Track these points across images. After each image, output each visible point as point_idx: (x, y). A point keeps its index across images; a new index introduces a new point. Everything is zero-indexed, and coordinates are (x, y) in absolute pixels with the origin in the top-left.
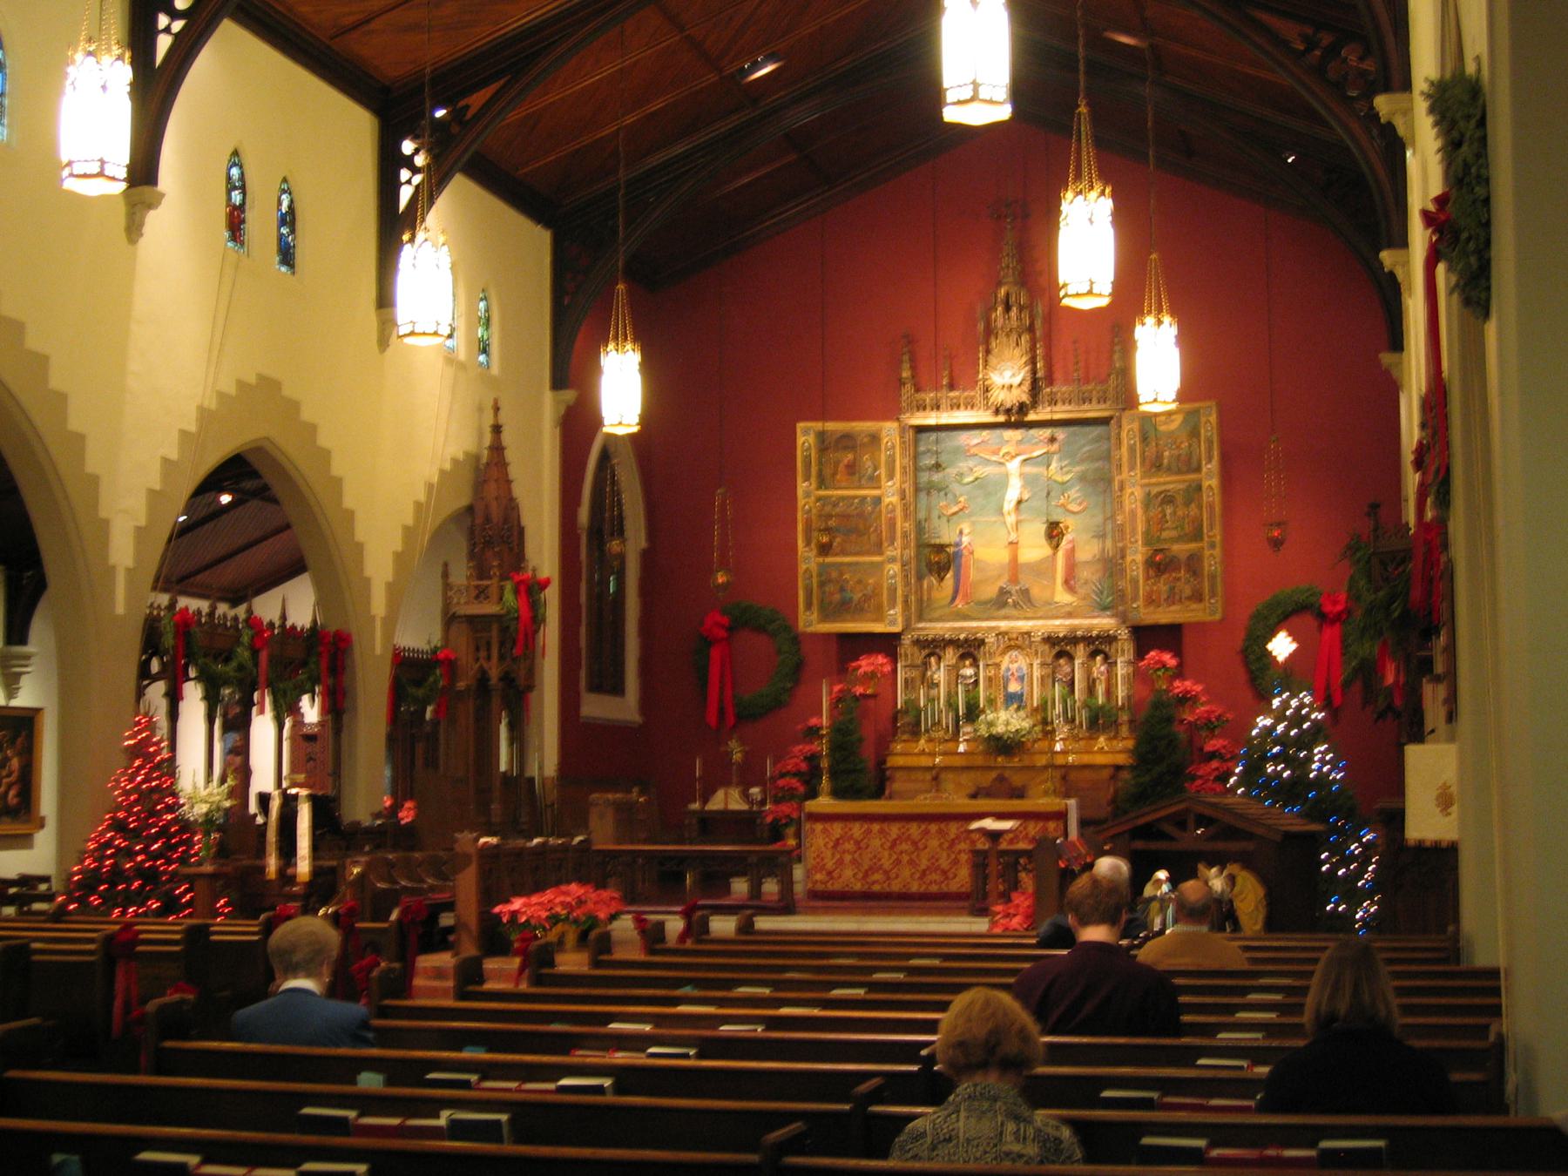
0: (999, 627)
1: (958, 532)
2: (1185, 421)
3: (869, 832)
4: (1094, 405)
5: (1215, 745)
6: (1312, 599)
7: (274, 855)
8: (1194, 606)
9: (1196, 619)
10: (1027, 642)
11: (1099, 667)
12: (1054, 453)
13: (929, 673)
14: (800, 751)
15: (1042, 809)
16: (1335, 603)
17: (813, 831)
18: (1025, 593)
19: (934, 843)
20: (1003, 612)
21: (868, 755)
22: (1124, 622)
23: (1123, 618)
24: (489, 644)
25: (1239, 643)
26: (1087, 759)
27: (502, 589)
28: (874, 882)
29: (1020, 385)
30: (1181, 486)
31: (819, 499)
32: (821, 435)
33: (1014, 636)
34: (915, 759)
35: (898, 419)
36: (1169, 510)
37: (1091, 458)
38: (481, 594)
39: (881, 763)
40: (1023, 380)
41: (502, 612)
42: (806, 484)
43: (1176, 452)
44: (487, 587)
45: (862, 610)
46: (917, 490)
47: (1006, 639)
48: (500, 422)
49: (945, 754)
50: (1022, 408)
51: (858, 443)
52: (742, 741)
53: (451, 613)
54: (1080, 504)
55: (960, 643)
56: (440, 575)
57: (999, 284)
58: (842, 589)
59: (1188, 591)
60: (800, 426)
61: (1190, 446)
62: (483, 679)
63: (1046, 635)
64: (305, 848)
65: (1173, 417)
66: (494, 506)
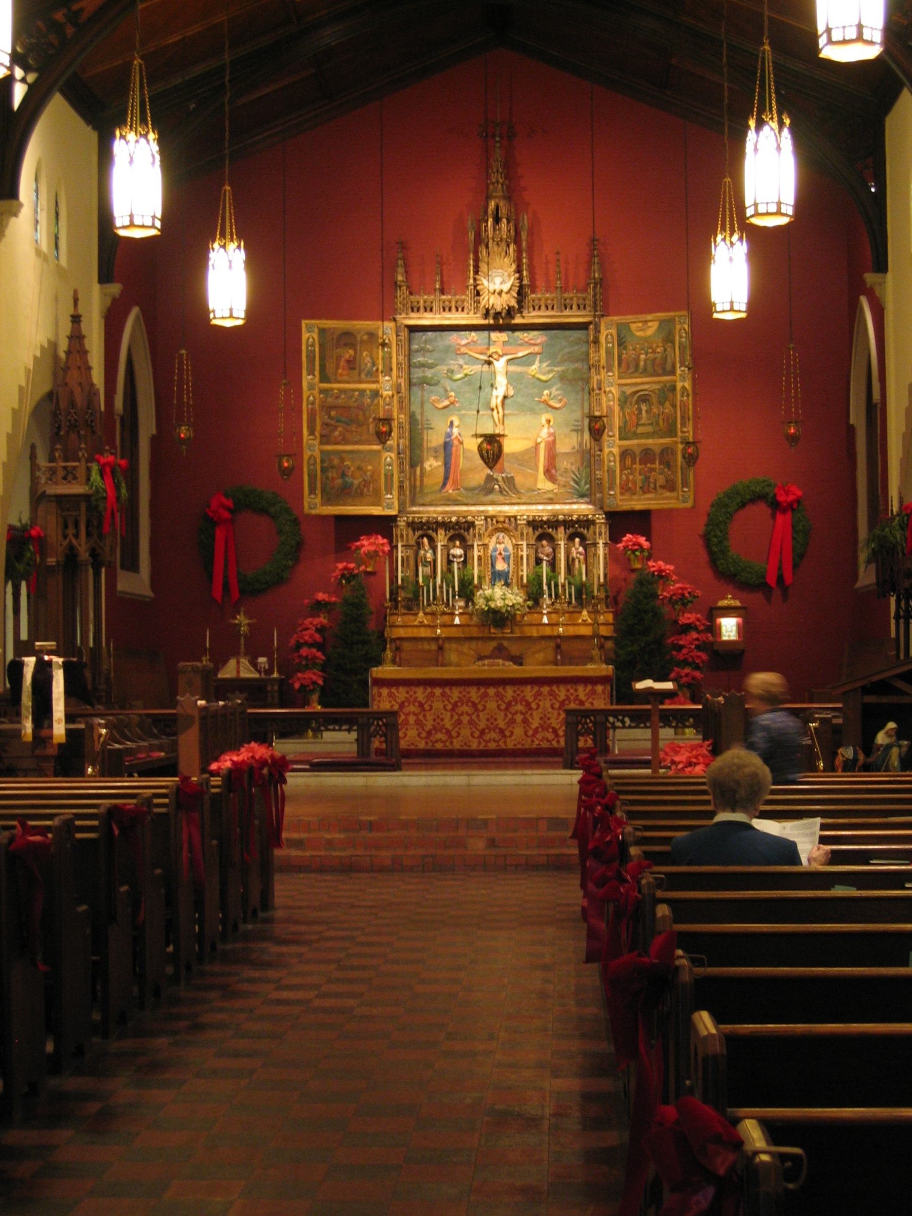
0: (487, 511)
1: (449, 424)
2: (660, 327)
3: (432, 695)
4: (575, 312)
5: (689, 619)
6: (767, 490)
7: (30, 718)
8: (668, 494)
9: (670, 506)
10: (513, 525)
11: (577, 549)
12: (537, 354)
13: (422, 552)
14: (311, 623)
15: (591, 674)
16: (787, 493)
17: (380, 695)
18: (510, 481)
19: (492, 705)
20: (491, 497)
21: (372, 626)
22: (601, 508)
23: (600, 505)
24: (77, 525)
25: (702, 529)
26: (572, 631)
27: (89, 470)
28: (437, 741)
29: (508, 292)
30: (655, 387)
31: (321, 391)
32: (322, 331)
33: (502, 519)
34: (415, 630)
35: (395, 320)
36: (644, 408)
37: (571, 358)
38: (69, 475)
39: (381, 635)
40: (512, 286)
41: (91, 492)
42: (310, 377)
43: (651, 356)
44: (75, 468)
45: (362, 494)
46: (410, 384)
47: (494, 522)
48: (80, 312)
49: (443, 626)
50: (510, 312)
51: (359, 339)
52: (248, 615)
53: (39, 492)
54: (560, 401)
55: (451, 525)
56: (28, 458)
57: (488, 198)
58: (343, 475)
59: (661, 480)
60: (304, 323)
61: (665, 350)
62: (71, 556)
63: (531, 519)
64: (61, 711)
65: (650, 324)
66: (77, 391)
